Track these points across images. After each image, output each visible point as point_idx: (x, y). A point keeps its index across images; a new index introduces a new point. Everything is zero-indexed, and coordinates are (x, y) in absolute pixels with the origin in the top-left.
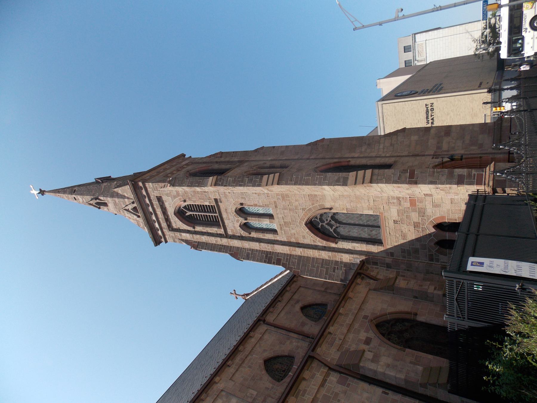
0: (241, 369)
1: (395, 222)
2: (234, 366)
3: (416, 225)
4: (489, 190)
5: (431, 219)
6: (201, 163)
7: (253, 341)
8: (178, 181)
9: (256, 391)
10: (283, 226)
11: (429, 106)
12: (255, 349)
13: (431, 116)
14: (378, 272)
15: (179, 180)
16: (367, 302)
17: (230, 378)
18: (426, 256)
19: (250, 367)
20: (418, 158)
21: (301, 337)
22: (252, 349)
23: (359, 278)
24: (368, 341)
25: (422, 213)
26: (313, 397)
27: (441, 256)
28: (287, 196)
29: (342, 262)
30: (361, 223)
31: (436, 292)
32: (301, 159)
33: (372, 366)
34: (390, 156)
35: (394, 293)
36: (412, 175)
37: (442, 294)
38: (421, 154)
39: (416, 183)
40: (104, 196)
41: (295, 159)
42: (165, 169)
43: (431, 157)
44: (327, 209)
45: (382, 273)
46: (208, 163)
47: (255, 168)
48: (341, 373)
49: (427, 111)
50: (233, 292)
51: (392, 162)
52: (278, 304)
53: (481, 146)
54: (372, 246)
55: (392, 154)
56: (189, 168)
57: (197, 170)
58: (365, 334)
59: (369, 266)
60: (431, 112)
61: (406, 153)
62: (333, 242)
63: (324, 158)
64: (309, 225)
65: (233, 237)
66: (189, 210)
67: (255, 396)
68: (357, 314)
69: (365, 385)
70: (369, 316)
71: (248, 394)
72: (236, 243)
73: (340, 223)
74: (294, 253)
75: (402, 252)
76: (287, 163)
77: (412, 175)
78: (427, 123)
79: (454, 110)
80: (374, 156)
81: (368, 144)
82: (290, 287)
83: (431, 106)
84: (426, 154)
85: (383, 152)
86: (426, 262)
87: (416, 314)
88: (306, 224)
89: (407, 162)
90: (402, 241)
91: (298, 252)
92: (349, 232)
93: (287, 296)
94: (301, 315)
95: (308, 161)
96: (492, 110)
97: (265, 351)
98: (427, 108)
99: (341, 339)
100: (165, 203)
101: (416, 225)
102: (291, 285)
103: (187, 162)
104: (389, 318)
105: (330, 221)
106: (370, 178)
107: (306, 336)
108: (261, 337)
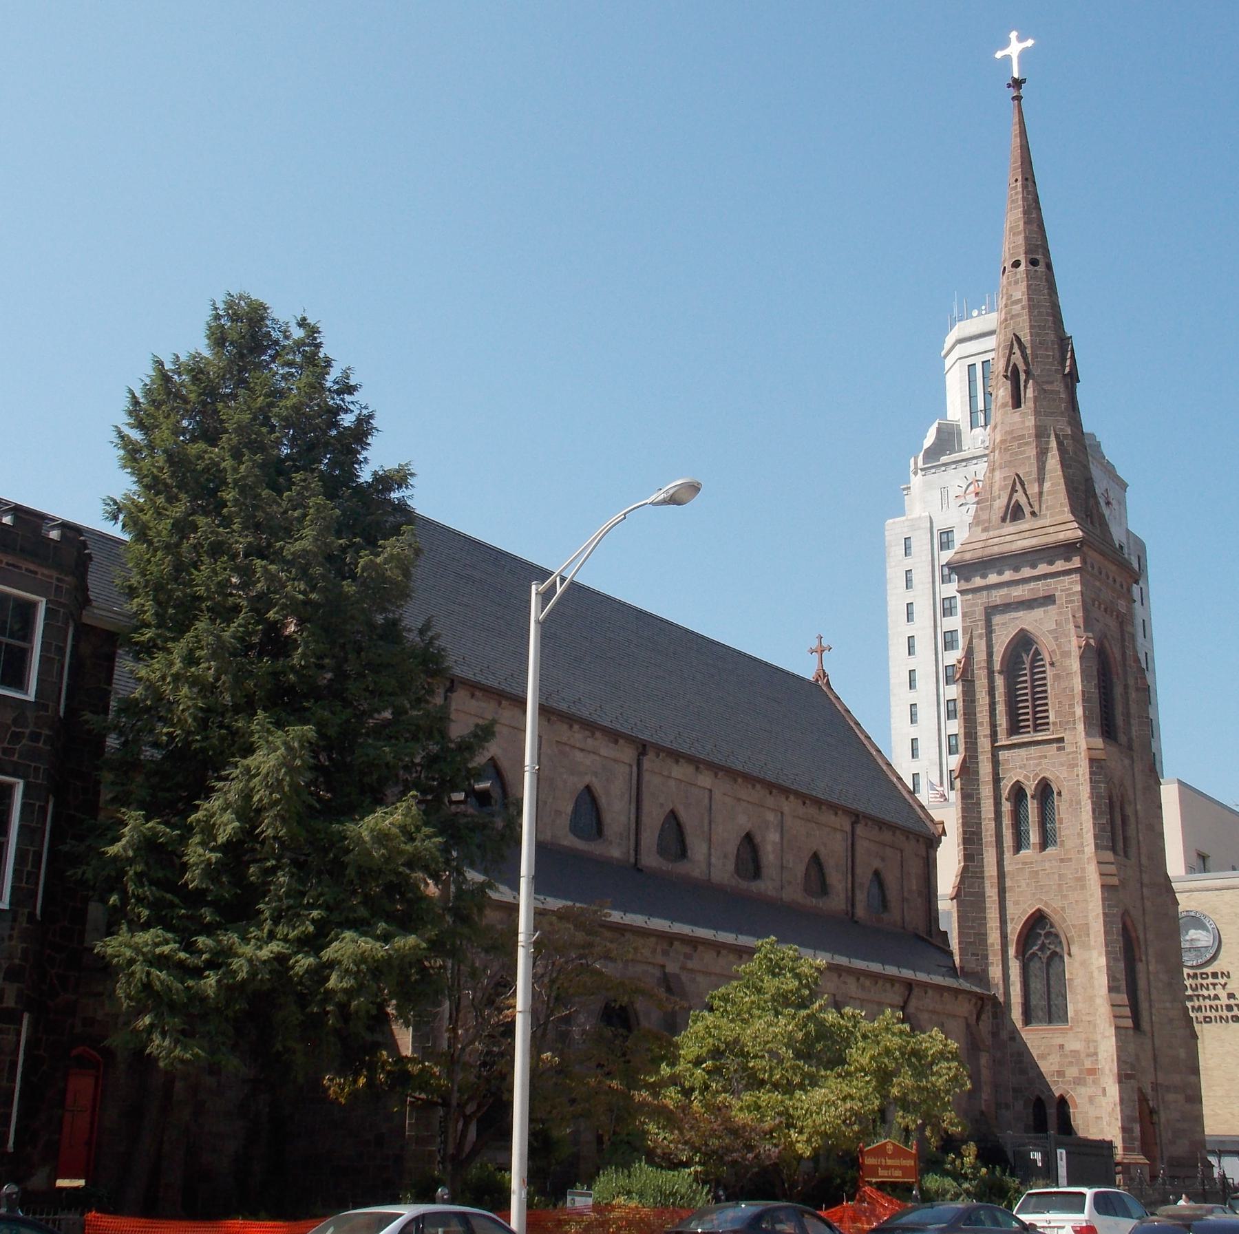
1: (1061, 1046)
3: (1061, 1074)
4: (1118, 1158)
25: (1079, 1081)
27: (1021, 1102)
28: (1083, 887)
29: (987, 965)
30: (1053, 996)
31: (983, 1102)
36: (1128, 1076)
39: (1120, 1082)
40: (1036, 399)
44: (1069, 950)
45: (985, 1026)
54: (1020, 1011)
62: (1017, 951)
64: (1038, 914)
65: (996, 763)
66: (1034, 660)
72: (985, 769)
73: (1048, 965)
74: (987, 883)
76: (1132, 851)
77: (1128, 1076)
88: (1039, 910)
90: (1034, 1053)
91: (991, 893)
92: (1036, 976)
100: (1043, 609)
101: (1061, 1074)
105: (1049, 949)
106: (1122, 1025)
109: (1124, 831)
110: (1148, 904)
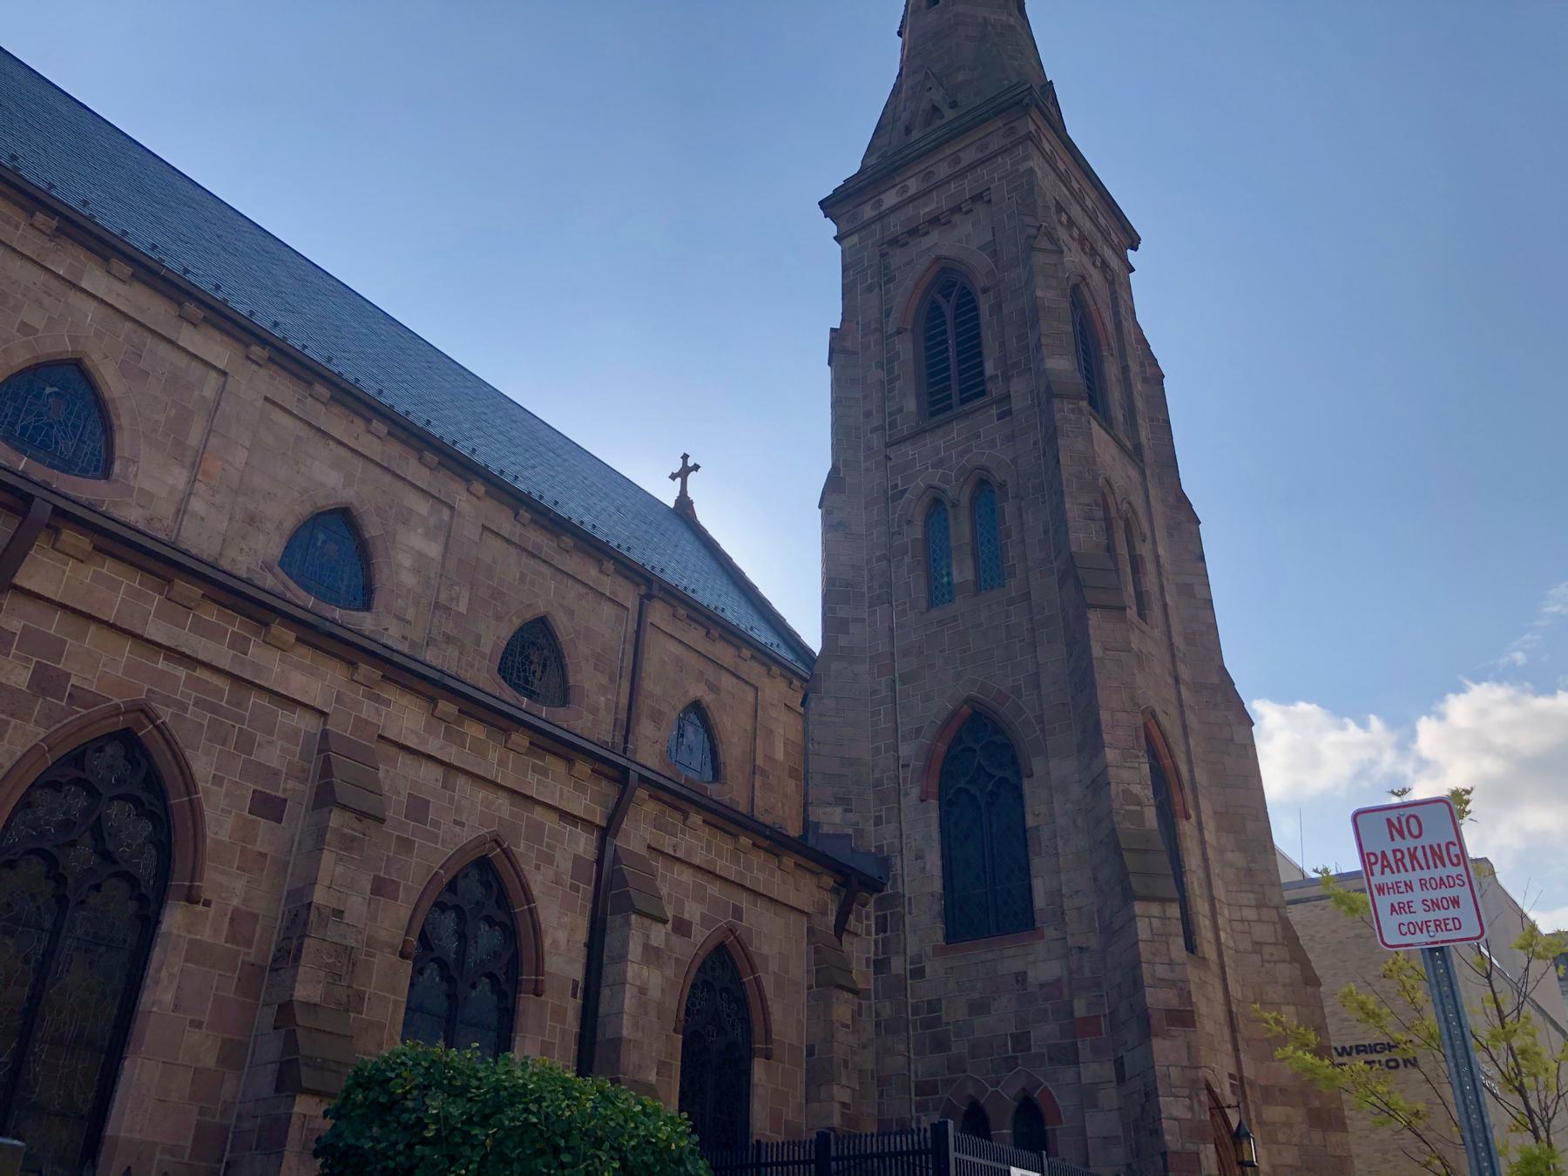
0: (513, 551)
1: (1021, 977)
2: (518, 529)
5: (1046, 1083)
6: (1116, 314)
7: (590, 573)
8: (1052, 262)
9: (467, 609)
12: (570, 582)
16: (775, 914)
17: (486, 524)
19: (523, 577)
20: (1226, 1031)
21: (623, 716)
24: (682, 927)
26: (534, 796)
32: (1173, 656)
33: (635, 950)
35: (810, 987)
37: (836, 1126)
38: (1239, 1038)
41: (1170, 638)
42: (1079, 198)
43: (1233, 1071)
47: (1125, 506)
48: (599, 861)
50: (690, 463)
51: (1204, 953)
55: (1228, 947)
56: (1096, 277)
57: (1093, 308)
58: (696, 919)
59: (871, 908)
61: (1235, 990)
63: (1186, 735)
64: (966, 710)
67: (456, 609)
68: (742, 886)
69: (582, 936)
70: (742, 921)
71: (457, 588)
75: (928, 1002)
76: (1156, 612)
78: (1340, 1050)
79: (1402, 1139)
80: (1215, 893)
81: (1250, 870)
82: (752, 657)
84: (1243, 1056)
85: (1231, 921)
86: (912, 1074)
87: (768, 1056)
89: (1208, 999)
94: (680, 707)
95: (1170, 680)
97: (571, 613)
99: (675, 851)
103: (1114, 262)
104: (745, 980)
107: (627, 729)
108: (604, 594)
110: (1191, 718)
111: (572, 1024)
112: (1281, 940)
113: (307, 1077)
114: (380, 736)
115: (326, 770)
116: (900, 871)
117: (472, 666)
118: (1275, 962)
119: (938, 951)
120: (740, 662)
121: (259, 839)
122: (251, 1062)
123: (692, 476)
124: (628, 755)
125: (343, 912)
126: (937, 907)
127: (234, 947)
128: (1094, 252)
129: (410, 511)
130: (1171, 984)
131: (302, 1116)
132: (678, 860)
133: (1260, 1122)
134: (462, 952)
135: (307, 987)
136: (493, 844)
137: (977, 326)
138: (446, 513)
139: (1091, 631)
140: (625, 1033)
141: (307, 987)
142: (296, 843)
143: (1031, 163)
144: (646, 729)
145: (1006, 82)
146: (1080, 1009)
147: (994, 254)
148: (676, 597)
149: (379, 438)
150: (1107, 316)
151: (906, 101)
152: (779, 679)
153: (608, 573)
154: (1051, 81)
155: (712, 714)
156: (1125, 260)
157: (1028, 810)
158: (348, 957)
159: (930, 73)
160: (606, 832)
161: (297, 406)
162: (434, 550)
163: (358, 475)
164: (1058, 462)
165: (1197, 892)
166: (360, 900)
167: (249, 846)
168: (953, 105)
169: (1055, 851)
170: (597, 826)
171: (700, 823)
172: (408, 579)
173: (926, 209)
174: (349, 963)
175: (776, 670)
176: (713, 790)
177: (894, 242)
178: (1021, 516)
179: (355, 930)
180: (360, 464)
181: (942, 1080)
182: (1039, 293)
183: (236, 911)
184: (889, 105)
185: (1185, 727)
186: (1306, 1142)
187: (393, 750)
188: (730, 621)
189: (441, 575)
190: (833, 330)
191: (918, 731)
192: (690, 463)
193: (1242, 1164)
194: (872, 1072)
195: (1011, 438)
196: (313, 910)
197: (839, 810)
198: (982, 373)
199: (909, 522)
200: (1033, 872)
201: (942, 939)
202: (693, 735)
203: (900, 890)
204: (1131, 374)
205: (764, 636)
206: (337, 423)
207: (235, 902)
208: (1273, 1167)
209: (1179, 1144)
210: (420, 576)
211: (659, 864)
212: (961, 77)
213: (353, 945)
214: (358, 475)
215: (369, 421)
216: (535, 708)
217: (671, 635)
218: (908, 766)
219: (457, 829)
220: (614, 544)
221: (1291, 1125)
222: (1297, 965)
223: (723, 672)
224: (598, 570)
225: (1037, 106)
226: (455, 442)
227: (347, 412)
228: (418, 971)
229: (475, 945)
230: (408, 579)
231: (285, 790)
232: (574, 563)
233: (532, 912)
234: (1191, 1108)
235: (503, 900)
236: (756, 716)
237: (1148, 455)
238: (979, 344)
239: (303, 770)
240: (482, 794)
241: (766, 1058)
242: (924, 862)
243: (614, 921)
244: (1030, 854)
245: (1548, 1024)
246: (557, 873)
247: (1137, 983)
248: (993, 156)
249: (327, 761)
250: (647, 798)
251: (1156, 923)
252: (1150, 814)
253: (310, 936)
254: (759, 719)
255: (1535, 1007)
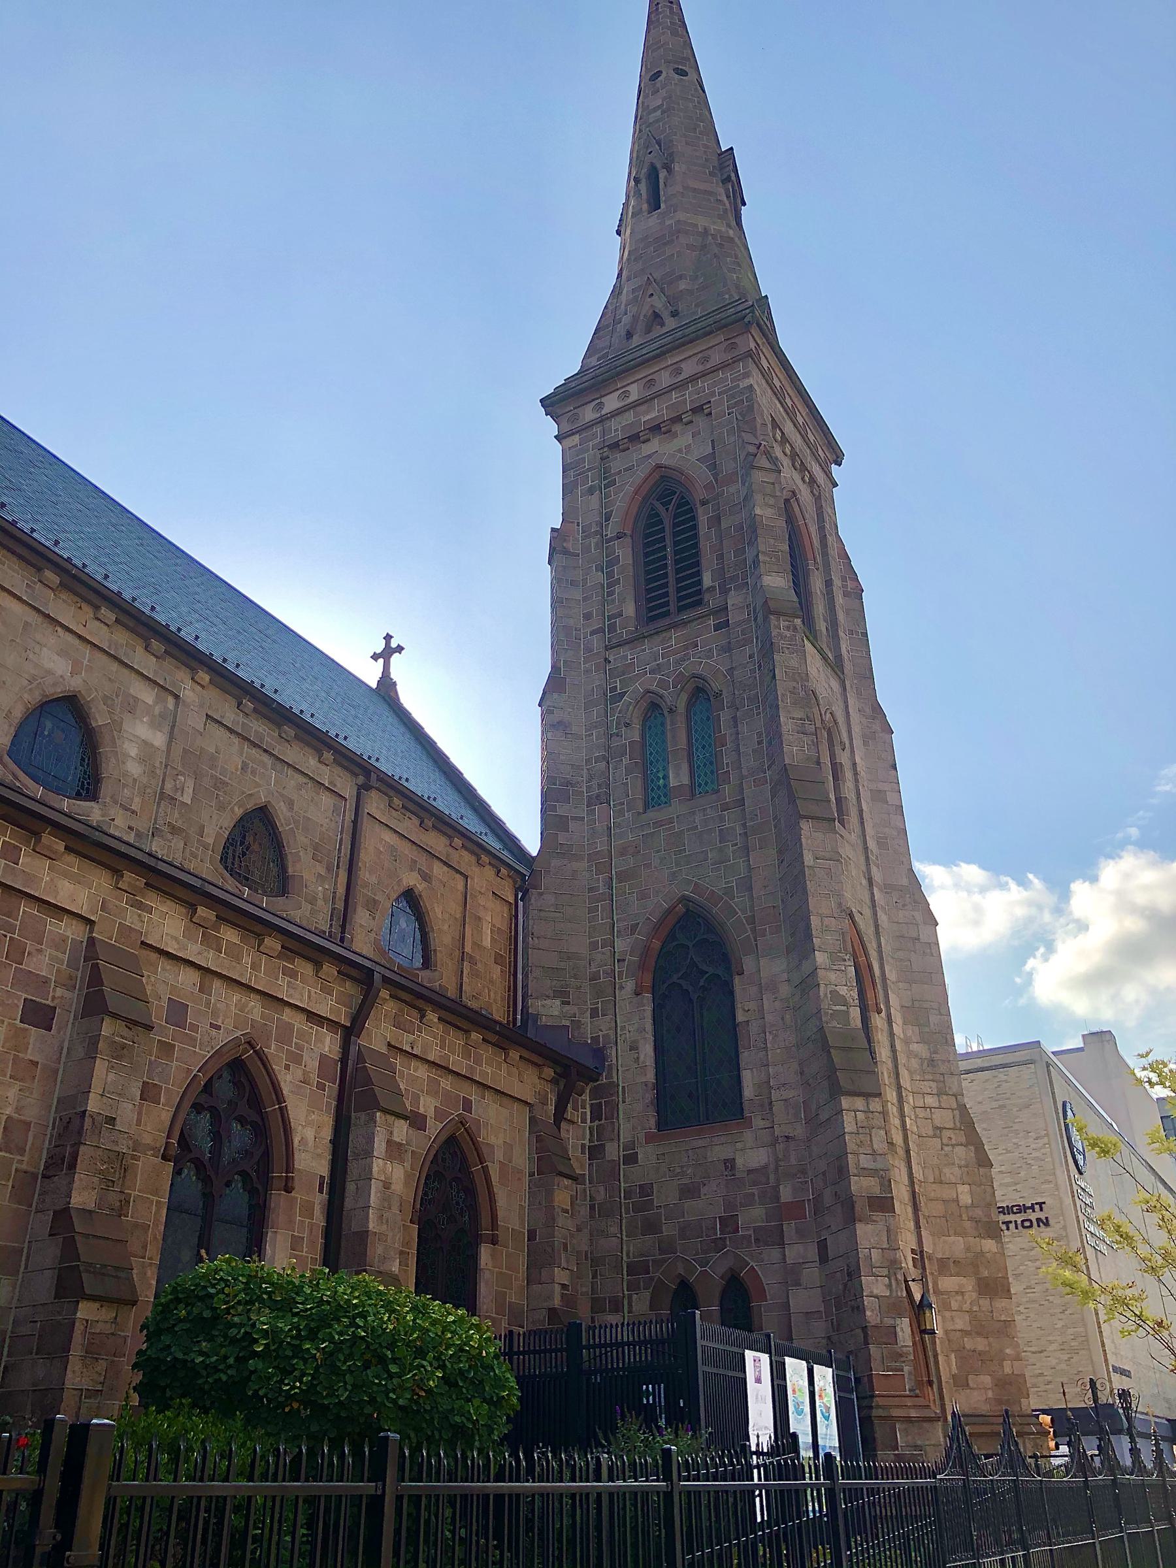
0: (236, 740)
1: (730, 1164)
2: (241, 718)
6: (821, 528)
7: (310, 763)
10: (669, 829)
11: (1038, 1214)
12: (290, 772)
13: (1007, 1223)
14: (573, 1123)
15: (773, 484)
18: (642, 1255)
19: (244, 767)
21: (340, 905)
22: (289, 765)
23: (555, 1072)
24: (417, 1121)
27: (647, 1295)
32: (867, 858)
33: (379, 1146)
34: (907, 1130)
35: (531, 1174)
41: (865, 842)
42: (790, 413)
46: (825, 554)
48: (344, 1060)
49: (1023, 1209)
50: (394, 644)
51: (892, 1139)
52: (413, 817)
53: (961, 1382)
55: (912, 1132)
56: (805, 494)
57: (801, 522)
59: (586, 1096)
60: (1019, 1222)
63: (877, 933)
68: (447, 1069)
69: (327, 1134)
76: (853, 819)
83: (1039, 1220)
87: (494, 1241)
93: (436, 842)
95: (864, 882)
96: (1045, 1412)
97: (290, 804)
98: (1032, 1207)
99: (412, 1048)
102: (467, 849)
107: (344, 918)
108: (323, 785)
109: (837, 788)
110: (883, 918)
111: (319, 1219)
112: (958, 1124)
113: (89, 1284)
114: (142, 943)
115: (95, 978)
116: (614, 1061)
117: (196, 857)
118: (953, 1146)
119: (650, 1138)
120: (451, 850)
121: (31, 1046)
122: (26, 1268)
123: (395, 658)
124: (345, 944)
125: (115, 1118)
126: (650, 1096)
127: (7, 1155)
128: (803, 469)
129: (136, 699)
130: (873, 1173)
131: (84, 1322)
132: (416, 1056)
133: (937, 1292)
134: (216, 1151)
135: (82, 1197)
136: (247, 1046)
137: (696, 536)
138: (171, 701)
139: (803, 840)
140: (371, 1226)
141: (82, 1197)
142: (65, 1051)
143: (751, 381)
144: (361, 917)
145: (727, 296)
146: (786, 1194)
147: (713, 467)
148: (391, 787)
149: (108, 626)
150: (813, 529)
151: (626, 306)
152: (488, 867)
153: (327, 762)
154: (766, 296)
155: (424, 902)
156: (829, 475)
157: (739, 1005)
158: (119, 1163)
159: (652, 280)
160: (350, 1032)
161: (26, 591)
162: (159, 739)
163: (85, 662)
164: (774, 676)
165: (887, 1082)
166: (131, 1106)
167: (21, 1055)
168: (674, 314)
169: (763, 1046)
170: (343, 1026)
171: (436, 1020)
172: (134, 769)
173: (650, 415)
174: (121, 1169)
175: (485, 859)
176: (424, 976)
177: (615, 446)
178: (736, 726)
179: (126, 1136)
180: (87, 651)
181: (652, 1260)
182: (758, 511)
183: (9, 1118)
184: (609, 306)
185: (877, 926)
186: (975, 1308)
187: (154, 956)
188: (442, 810)
189: (166, 766)
190: (553, 530)
191: (634, 928)
192: (394, 644)
193: (923, 1332)
194: (586, 1252)
195: (727, 649)
196: (88, 1120)
197: (558, 1002)
198: (700, 582)
199: (627, 725)
200: (742, 1065)
201: (653, 1127)
202: (406, 924)
203: (615, 1080)
204: (834, 589)
205: (472, 823)
206: (65, 610)
207: (8, 1111)
208: (946, 1332)
209: (879, 1319)
210: (145, 765)
211: (398, 1061)
212: (683, 285)
213: (124, 1151)
214: (85, 662)
215: (97, 608)
216: (256, 898)
217: (387, 825)
218: (624, 960)
219: (214, 1032)
220: (332, 734)
221: (963, 1293)
222: (972, 1148)
223: (435, 860)
224: (317, 759)
225: (758, 325)
226: (179, 630)
227: (76, 599)
228: (177, 1172)
229: (228, 1144)
230: (134, 769)
231: (54, 998)
232: (294, 753)
233: (283, 1111)
234: (890, 1286)
235: (256, 1102)
236: (466, 903)
237: (848, 666)
238: (697, 554)
239: (71, 978)
240: (236, 997)
241: (492, 1244)
242: (638, 1053)
243: (356, 1117)
244: (740, 1048)
245: (1159, 1184)
246: (305, 1073)
247: (842, 1172)
248: (714, 370)
249: (95, 967)
250: (388, 998)
251: (860, 1115)
252: (855, 1013)
253: (85, 1144)
254: (468, 908)
255: (1148, 1168)
